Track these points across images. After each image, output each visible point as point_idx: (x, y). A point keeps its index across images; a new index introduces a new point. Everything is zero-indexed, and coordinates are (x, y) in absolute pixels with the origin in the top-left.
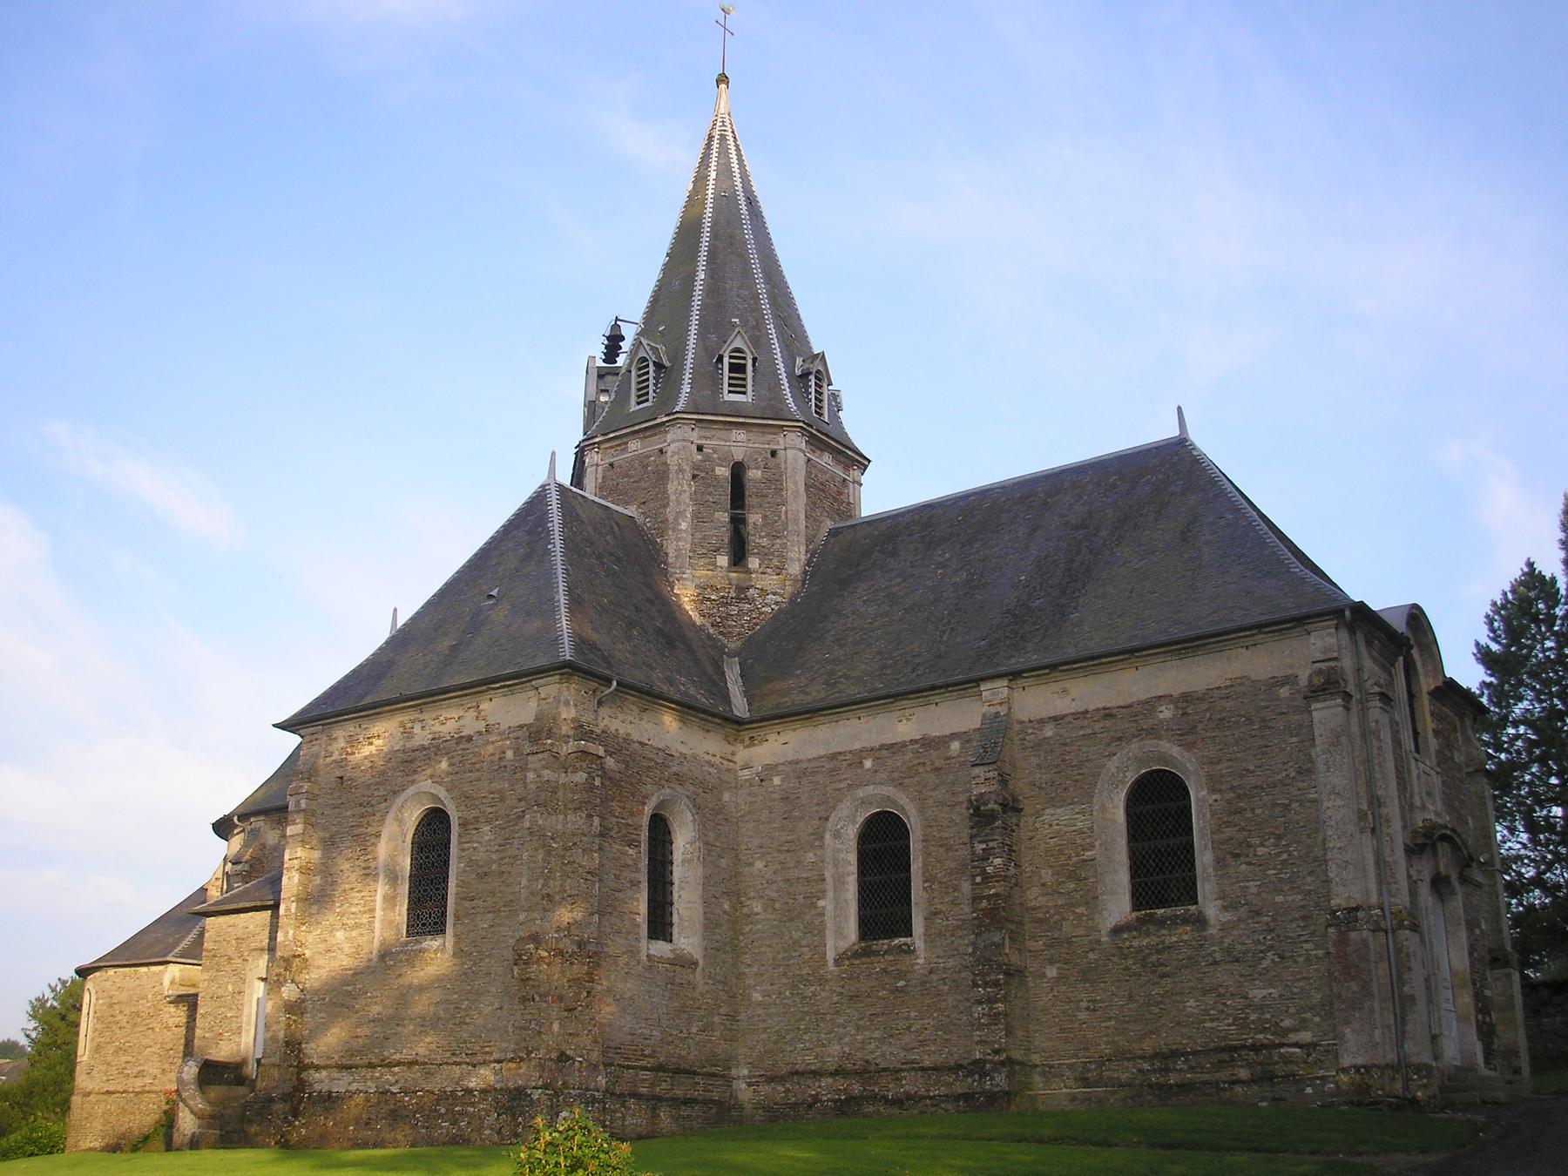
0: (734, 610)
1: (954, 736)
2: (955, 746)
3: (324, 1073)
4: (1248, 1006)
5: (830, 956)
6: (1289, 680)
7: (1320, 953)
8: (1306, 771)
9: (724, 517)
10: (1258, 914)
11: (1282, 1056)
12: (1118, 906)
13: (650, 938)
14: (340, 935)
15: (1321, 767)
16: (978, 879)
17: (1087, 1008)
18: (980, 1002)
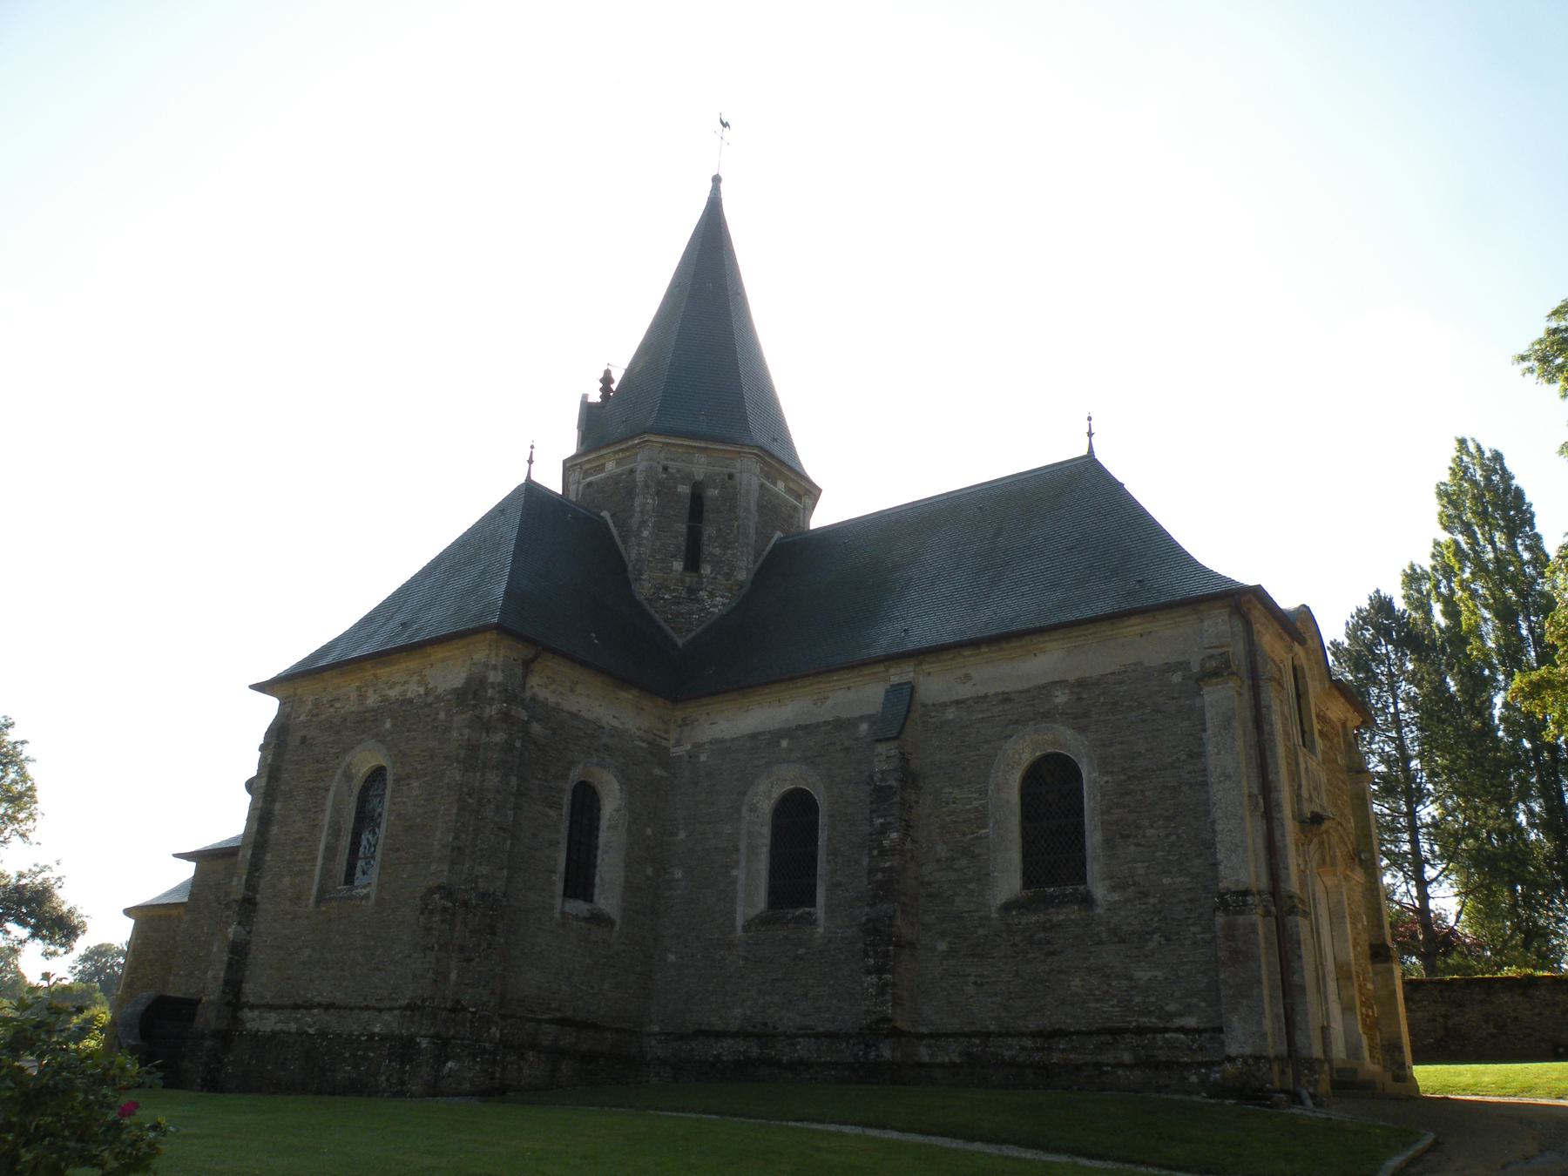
0: (683, 609)
1: (863, 718)
2: (864, 727)
3: (256, 1012)
4: (1133, 988)
5: (740, 921)
6: (1183, 666)
7: (1208, 936)
8: (1197, 754)
9: (682, 528)
10: (1146, 895)
11: (1165, 1039)
12: (1008, 882)
13: (565, 894)
14: (286, 880)
15: (1211, 749)
16: (875, 853)
17: (975, 983)
18: (869, 973)
